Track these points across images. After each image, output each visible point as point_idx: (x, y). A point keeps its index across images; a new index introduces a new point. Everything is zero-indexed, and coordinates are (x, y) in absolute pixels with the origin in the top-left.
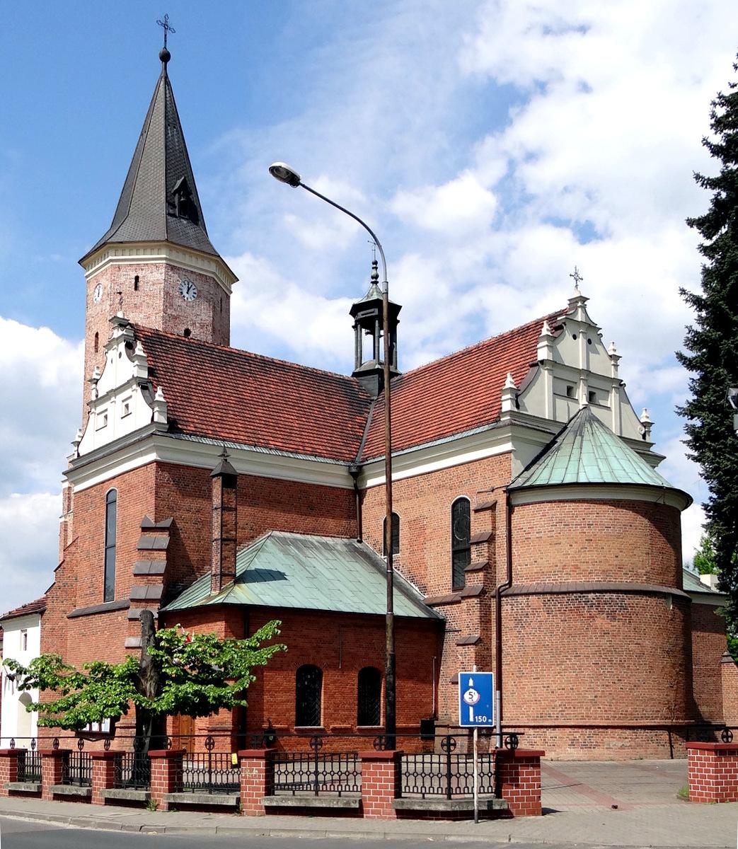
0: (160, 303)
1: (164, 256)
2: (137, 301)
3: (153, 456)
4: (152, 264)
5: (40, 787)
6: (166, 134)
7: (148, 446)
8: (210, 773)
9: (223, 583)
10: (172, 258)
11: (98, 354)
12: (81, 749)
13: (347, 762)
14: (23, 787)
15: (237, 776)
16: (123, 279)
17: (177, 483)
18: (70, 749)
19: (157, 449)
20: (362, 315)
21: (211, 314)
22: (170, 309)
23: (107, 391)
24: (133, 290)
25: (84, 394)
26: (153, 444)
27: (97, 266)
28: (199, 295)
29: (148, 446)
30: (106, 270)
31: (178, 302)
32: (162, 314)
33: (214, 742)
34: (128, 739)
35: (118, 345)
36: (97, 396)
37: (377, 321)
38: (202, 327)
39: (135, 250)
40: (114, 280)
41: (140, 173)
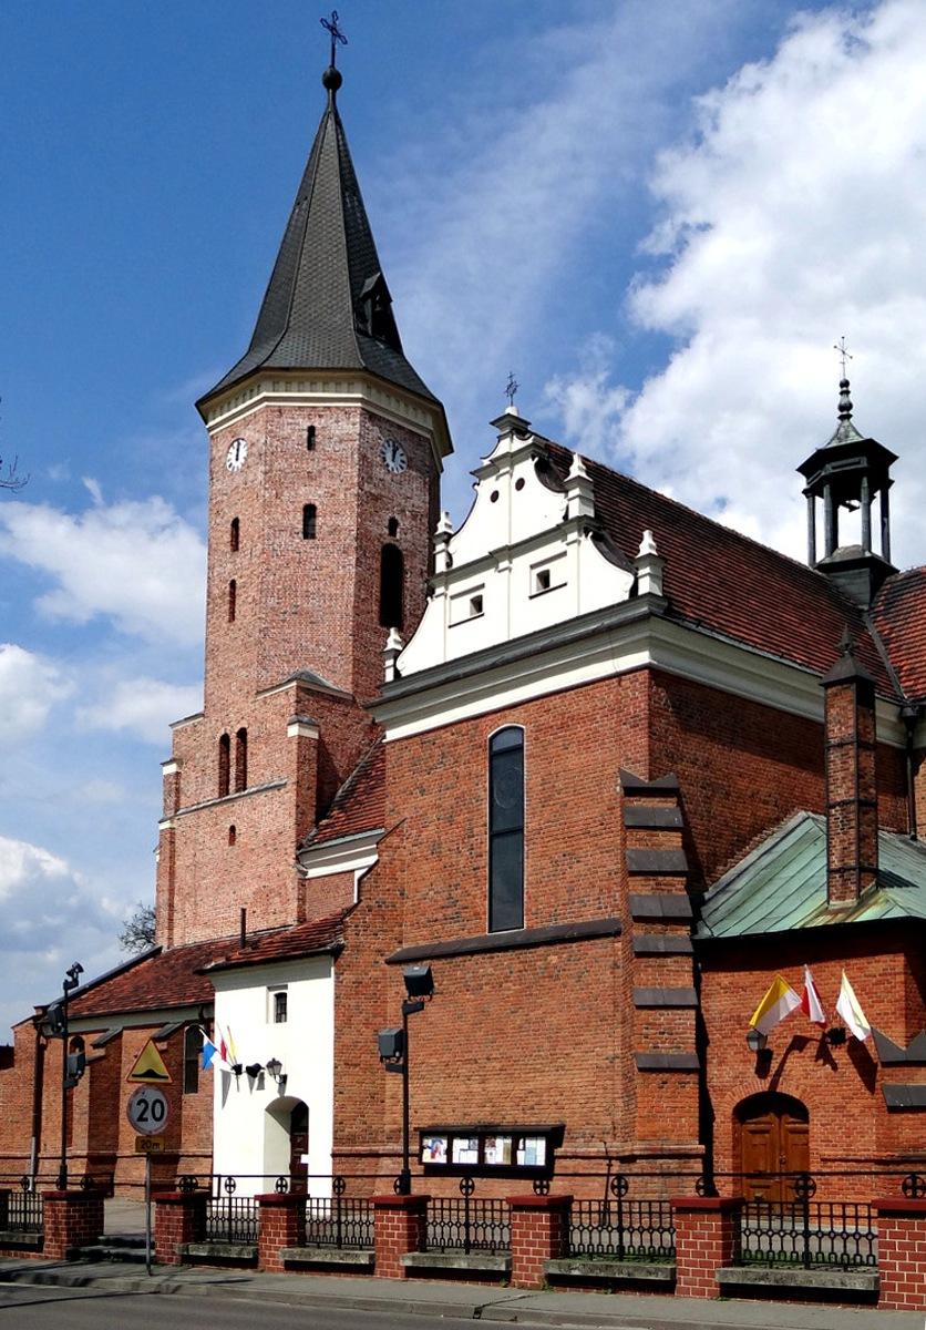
0: (352, 472)
1: (360, 396)
2: (313, 467)
3: (642, 658)
4: (337, 408)
5: (256, 1253)
6: (344, 203)
7: (629, 640)
8: (467, 1225)
9: (862, 884)
10: (371, 400)
11: (240, 553)
12: (230, 1192)
13: (793, 1216)
14: (202, 1251)
15: (607, 1234)
16: (287, 431)
17: (678, 710)
18: (567, 1194)
19: (652, 644)
20: (834, 468)
21: (427, 497)
22: (369, 483)
23: (492, 549)
24: (305, 449)
25: (208, 621)
26: (647, 634)
27: (234, 411)
28: (410, 464)
29: (629, 640)
30: (255, 415)
31: (379, 472)
32: (355, 490)
33: (344, 1184)
34: (656, 1179)
35: (512, 466)
36: (449, 564)
37: (865, 480)
38: (414, 517)
39: (307, 384)
40: (271, 431)
41: (303, 262)
